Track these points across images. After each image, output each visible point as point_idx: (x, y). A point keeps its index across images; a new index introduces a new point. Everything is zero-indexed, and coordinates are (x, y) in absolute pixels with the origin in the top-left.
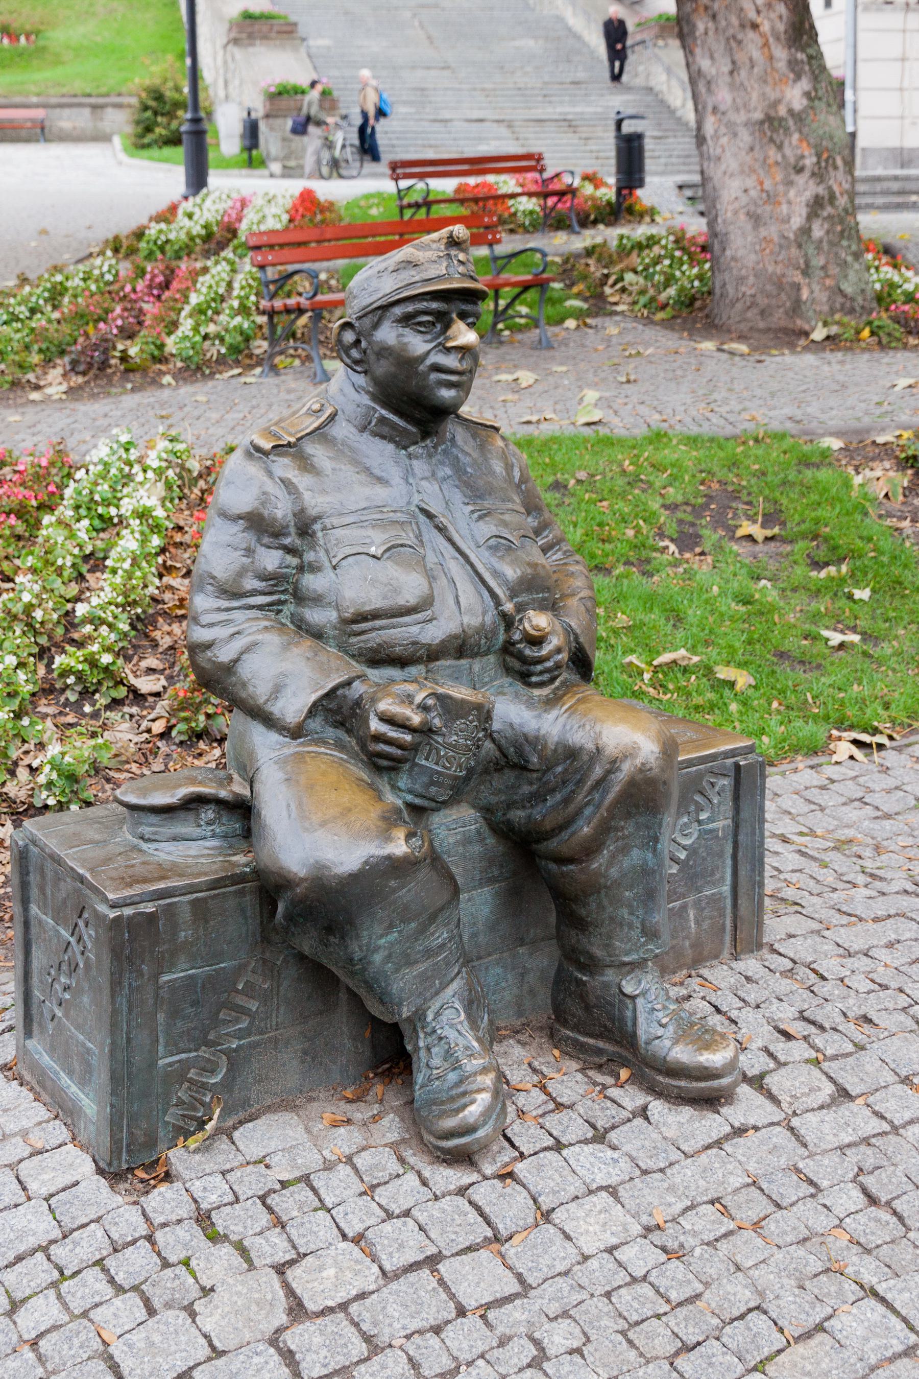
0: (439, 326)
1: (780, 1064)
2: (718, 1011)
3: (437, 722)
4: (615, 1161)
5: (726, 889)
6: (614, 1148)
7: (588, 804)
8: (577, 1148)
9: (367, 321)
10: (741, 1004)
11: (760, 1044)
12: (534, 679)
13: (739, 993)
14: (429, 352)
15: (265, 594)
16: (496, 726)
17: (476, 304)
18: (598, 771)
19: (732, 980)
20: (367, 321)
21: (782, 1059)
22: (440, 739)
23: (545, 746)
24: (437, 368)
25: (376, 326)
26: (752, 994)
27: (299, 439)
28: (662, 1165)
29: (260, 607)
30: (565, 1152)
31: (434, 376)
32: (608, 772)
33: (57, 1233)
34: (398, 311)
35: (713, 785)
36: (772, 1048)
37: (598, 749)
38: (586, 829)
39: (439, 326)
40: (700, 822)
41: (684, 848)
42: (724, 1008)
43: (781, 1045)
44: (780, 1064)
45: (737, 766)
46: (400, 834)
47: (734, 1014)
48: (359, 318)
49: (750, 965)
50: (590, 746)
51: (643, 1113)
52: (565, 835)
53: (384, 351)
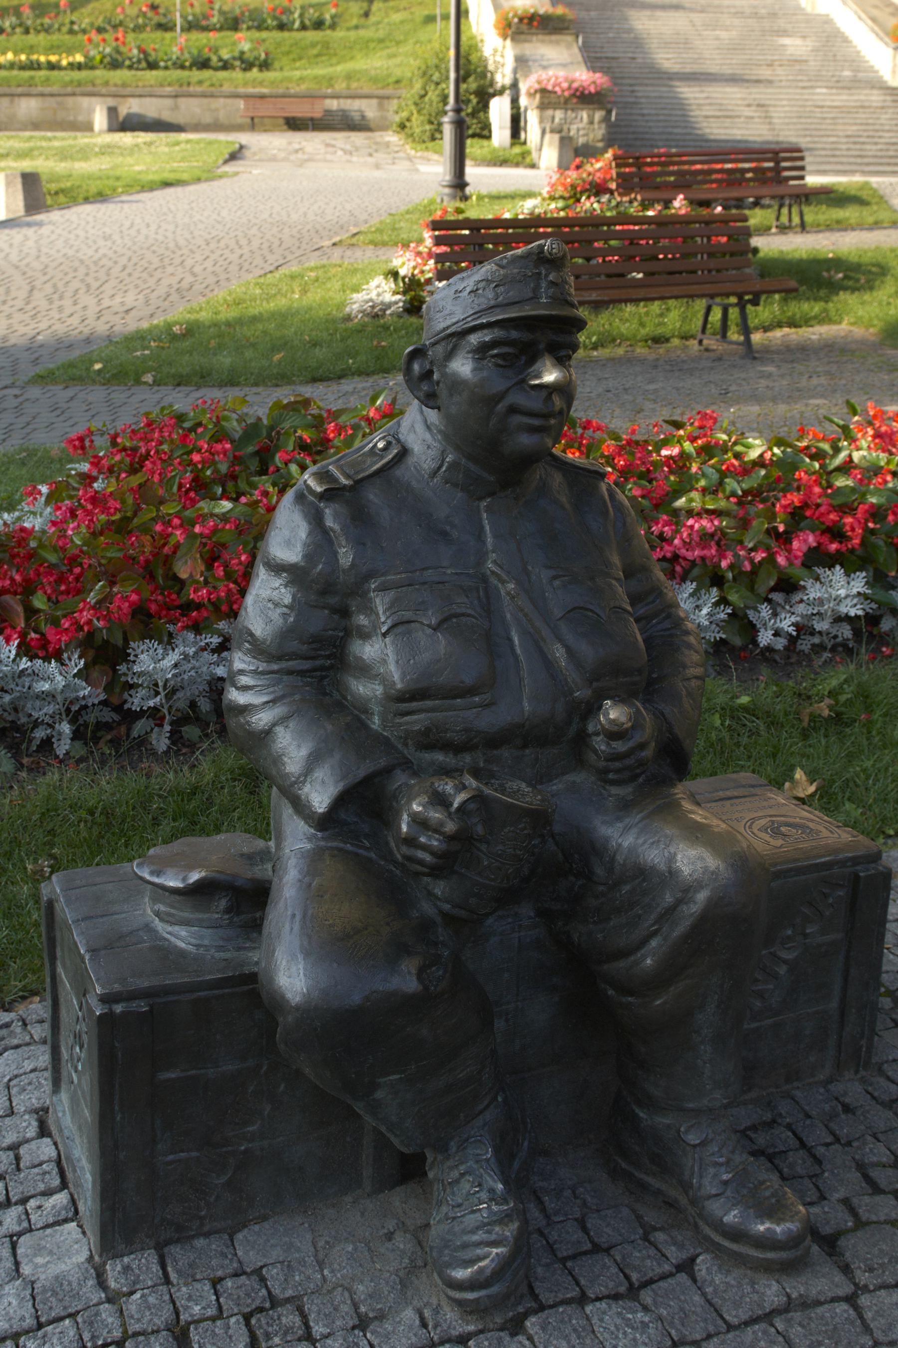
0: (524, 358)
1: (860, 1224)
2: (803, 1145)
3: (480, 830)
4: (645, 1325)
5: (834, 1004)
6: (646, 1309)
7: (654, 934)
8: (603, 1305)
9: (440, 349)
10: (829, 1139)
11: (841, 1194)
12: (611, 776)
13: (832, 1125)
14: (508, 390)
15: (306, 658)
16: (557, 828)
17: (571, 333)
18: (669, 899)
19: (827, 1107)
20: (440, 349)
21: (864, 1216)
22: (484, 847)
23: (613, 859)
24: (513, 410)
25: (450, 355)
26: (845, 1127)
27: (358, 482)
28: (698, 1337)
29: (290, 672)
30: (589, 1309)
31: (518, 419)
32: (679, 902)
33: (30, 1322)
34: (474, 339)
35: (825, 896)
36: (855, 1201)
37: (670, 872)
38: (649, 961)
39: (524, 358)
40: (806, 936)
41: (785, 962)
42: (810, 1142)
43: (867, 1199)
44: (860, 1224)
45: (857, 877)
46: (409, 966)
47: (820, 1151)
48: (434, 344)
49: (851, 1089)
50: (663, 867)
51: (687, 1266)
52: (622, 964)
53: (456, 384)
